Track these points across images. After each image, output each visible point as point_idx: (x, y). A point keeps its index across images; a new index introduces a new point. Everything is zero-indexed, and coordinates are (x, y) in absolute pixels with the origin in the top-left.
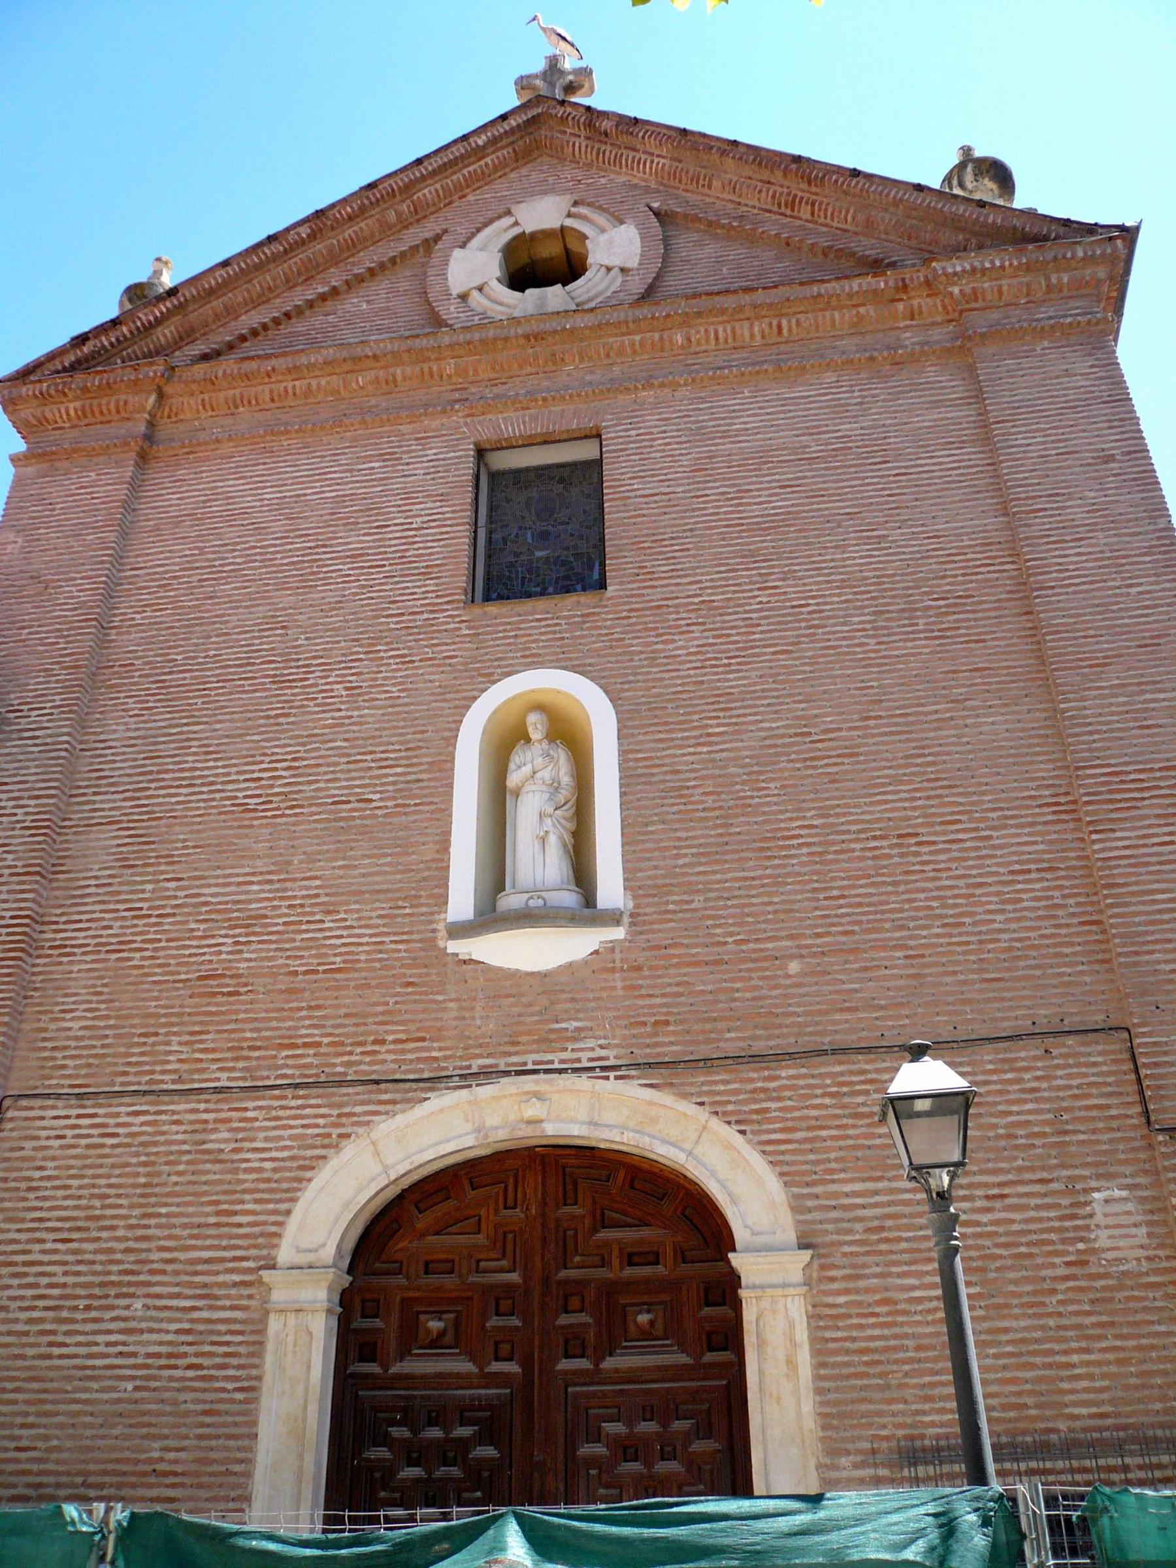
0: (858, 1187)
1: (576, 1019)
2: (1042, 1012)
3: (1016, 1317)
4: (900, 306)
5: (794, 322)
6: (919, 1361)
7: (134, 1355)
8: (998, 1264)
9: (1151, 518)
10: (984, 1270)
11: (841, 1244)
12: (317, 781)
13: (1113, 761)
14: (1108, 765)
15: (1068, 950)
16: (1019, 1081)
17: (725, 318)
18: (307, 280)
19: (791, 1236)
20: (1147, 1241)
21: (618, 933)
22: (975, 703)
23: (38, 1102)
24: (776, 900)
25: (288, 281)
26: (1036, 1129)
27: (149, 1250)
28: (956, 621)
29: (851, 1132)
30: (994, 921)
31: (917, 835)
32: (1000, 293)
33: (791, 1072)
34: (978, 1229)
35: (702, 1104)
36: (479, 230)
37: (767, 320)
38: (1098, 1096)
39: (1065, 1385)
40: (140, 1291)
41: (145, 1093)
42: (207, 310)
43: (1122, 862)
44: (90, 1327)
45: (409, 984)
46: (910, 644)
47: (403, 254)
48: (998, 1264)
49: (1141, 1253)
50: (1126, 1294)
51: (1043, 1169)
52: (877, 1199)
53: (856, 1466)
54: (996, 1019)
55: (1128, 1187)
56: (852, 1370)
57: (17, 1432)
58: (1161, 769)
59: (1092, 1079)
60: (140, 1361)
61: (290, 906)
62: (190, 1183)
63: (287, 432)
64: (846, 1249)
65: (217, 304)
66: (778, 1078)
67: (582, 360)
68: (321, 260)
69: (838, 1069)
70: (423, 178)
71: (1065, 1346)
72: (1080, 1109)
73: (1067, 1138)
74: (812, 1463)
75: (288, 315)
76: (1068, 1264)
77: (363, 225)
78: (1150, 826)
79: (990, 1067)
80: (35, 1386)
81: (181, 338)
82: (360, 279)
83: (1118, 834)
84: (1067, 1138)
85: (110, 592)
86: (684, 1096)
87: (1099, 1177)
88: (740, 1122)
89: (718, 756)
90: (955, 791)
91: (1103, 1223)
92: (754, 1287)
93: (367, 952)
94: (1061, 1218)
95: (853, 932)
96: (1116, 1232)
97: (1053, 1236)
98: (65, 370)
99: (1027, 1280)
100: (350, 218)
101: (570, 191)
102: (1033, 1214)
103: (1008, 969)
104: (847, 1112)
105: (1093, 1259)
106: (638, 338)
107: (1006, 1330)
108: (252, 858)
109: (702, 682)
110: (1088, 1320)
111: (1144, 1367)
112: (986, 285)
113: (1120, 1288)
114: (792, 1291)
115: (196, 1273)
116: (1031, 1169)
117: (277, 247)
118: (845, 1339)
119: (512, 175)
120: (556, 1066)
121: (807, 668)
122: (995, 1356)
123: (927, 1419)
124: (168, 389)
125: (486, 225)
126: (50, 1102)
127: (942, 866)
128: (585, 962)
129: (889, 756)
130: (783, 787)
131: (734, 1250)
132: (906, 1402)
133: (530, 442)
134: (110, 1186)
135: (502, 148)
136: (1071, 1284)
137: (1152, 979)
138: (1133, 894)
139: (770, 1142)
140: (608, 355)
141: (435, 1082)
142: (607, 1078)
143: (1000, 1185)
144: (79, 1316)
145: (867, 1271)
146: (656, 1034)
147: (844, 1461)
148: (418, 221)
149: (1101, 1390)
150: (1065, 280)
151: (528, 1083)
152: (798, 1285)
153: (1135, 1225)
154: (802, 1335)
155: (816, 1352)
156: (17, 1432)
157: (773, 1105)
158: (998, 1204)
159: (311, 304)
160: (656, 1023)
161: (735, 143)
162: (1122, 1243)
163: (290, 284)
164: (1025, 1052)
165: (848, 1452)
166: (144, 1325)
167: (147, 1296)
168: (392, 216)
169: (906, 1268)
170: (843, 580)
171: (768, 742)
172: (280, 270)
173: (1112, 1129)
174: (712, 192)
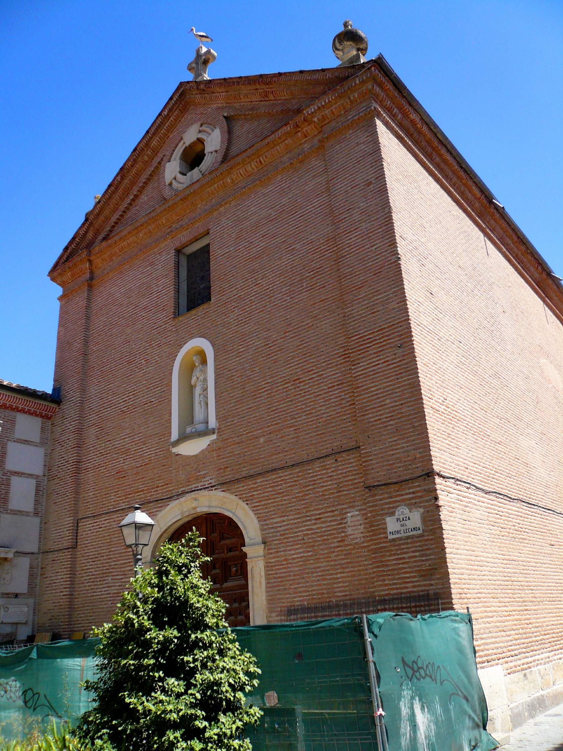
0: (279, 520)
1: (205, 470)
2: (335, 444)
3: (322, 562)
4: (299, 134)
5: (264, 157)
6: (294, 580)
7: (110, 594)
8: (318, 543)
9: (382, 209)
10: (313, 546)
11: (274, 540)
12: (139, 398)
13: (361, 332)
14: (359, 334)
15: (345, 417)
16: (326, 473)
17: (240, 166)
18: (127, 195)
19: (260, 540)
20: (363, 531)
21: (214, 437)
22: (321, 316)
23: (85, 520)
24: (257, 415)
25: (121, 199)
26: (331, 491)
27: (110, 562)
28: (316, 280)
29: (277, 500)
30: (322, 410)
31: (299, 379)
32: (333, 113)
33: (260, 480)
34: (312, 531)
35: (236, 495)
36: (174, 151)
37: (255, 160)
38: (351, 476)
39: (335, 586)
40: (110, 575)
41: (107, 513)
42: (100, 221)
43: (361, 377)
44: (101, 586)
45: (164, 465)
46: (300, 296)
47: (153, 171)
48: (318, 543)
49: (362, 535)
50: (356, 551)
51: (333, 506)
52: (284, 523)
53: (276, 616)
54: (320, 450)
55: (360, 510)
56: (276, 584)
57: (89, 618)
58: (377, 331)
59: (350, 469)
60: (111, 595)
61: (135, 444)
62: (118, 540)
63: (124, 264)
64: (275, 542)
65: (102, 218)
66: (256, 483)
67: (202, 201)
68: (128, 185)
69: (273, 477)
70: (151, 138)
71: (336, 572)
72: (345, 481)
73: (341, 494)
74: (265, 615)
75: (124, 212)
76: (339, 541)
77: (137, 166)
78: (372, 358)
79: (318, 469)
80: (91, 605)
81: (96, 234)
82: (143, 187)
83: (361, 364)
84: (341, 494)
85: (86, 342)
86: (232, 493)
87: (351, 507)
88: (246, 500)
89: (241, 361)
90: (312, 357)
91: (350, 525)
92: (251, 558)
93: (154, 456)
94: (337, 525)
95: (279, 423)
96: (354, 528)
97: (335, 532)
98: (65, 261)
99: (326, 549)
100: (132, 166)
101: (195, 122)
102: (329, 524)
103: (326, 429)
104: (276, 492)
105: (346, 539)
106: (216, 185)
107: (319, 567)
108: (125, 429)
109: (237, 331)
110: (343, 562)
111: (359, 578)
112: (327, 112)
113: (354, 549)
114: (259, 559)
115: (122, 568)
116: (329, 507)
117: (113, 188)
118: (274, 574)
119: (183, 120)
120: (200, 488)
121: (268, 316)
122: (316, 577)
123: (296, 599)
124: (91, 258)
125: (176, 147)
126: (88, 519)
127: (307, 390)
128: (206, 449)
129: (292, 347)
130: (260, 369)
131: (244, 546)
132: (290, 594)
133: (191, 242)
134: (102, 543)
135: (175, 111)
136: (339, 549)
137: (367, 425)
138: (363, 390)
139: (255, 507)
140: (209, 196)
141: (170, 498)
142: (212, 490)
143: (320, 514)
144: (98, 583)
145: (281, 550)
146: (225, 472)
147: (274, 615)
148: (156, 155)
149: (346, 587)
150: (356, 96)
151: (193, 495)
152: (262, 556)
153: (361, 525)
154: (263, 574)
155: (267, 579)
156: (89, 618)
157: (256, 493)
158: (318, 521)
159: (130, 204)
160: (224, 468)
161: (240, 77)
162: (356, 532)
163: (122, 199)
164: (329, 461)
165: (275, 612)
166: (112, 585)
167: (112, 576)
168: (146, 158)
169: (291, 548)
170: (280, 273)
171: (256, 351)
172: (117, 196)
173: (355, 488)
174: (243, 100)
